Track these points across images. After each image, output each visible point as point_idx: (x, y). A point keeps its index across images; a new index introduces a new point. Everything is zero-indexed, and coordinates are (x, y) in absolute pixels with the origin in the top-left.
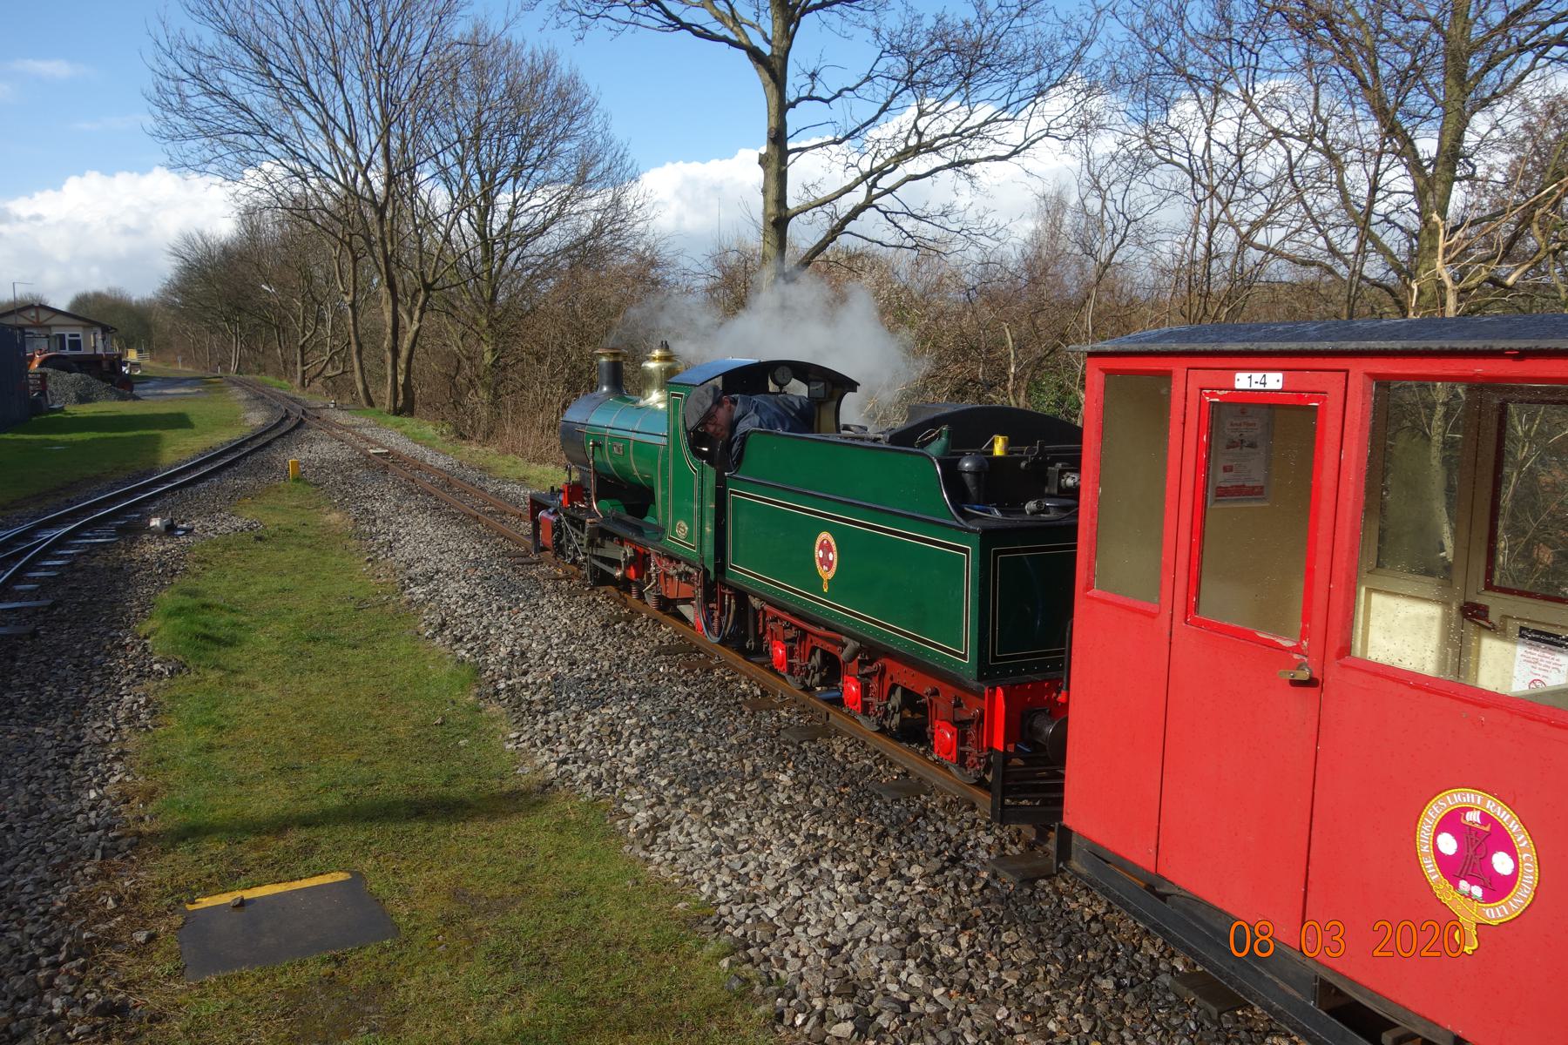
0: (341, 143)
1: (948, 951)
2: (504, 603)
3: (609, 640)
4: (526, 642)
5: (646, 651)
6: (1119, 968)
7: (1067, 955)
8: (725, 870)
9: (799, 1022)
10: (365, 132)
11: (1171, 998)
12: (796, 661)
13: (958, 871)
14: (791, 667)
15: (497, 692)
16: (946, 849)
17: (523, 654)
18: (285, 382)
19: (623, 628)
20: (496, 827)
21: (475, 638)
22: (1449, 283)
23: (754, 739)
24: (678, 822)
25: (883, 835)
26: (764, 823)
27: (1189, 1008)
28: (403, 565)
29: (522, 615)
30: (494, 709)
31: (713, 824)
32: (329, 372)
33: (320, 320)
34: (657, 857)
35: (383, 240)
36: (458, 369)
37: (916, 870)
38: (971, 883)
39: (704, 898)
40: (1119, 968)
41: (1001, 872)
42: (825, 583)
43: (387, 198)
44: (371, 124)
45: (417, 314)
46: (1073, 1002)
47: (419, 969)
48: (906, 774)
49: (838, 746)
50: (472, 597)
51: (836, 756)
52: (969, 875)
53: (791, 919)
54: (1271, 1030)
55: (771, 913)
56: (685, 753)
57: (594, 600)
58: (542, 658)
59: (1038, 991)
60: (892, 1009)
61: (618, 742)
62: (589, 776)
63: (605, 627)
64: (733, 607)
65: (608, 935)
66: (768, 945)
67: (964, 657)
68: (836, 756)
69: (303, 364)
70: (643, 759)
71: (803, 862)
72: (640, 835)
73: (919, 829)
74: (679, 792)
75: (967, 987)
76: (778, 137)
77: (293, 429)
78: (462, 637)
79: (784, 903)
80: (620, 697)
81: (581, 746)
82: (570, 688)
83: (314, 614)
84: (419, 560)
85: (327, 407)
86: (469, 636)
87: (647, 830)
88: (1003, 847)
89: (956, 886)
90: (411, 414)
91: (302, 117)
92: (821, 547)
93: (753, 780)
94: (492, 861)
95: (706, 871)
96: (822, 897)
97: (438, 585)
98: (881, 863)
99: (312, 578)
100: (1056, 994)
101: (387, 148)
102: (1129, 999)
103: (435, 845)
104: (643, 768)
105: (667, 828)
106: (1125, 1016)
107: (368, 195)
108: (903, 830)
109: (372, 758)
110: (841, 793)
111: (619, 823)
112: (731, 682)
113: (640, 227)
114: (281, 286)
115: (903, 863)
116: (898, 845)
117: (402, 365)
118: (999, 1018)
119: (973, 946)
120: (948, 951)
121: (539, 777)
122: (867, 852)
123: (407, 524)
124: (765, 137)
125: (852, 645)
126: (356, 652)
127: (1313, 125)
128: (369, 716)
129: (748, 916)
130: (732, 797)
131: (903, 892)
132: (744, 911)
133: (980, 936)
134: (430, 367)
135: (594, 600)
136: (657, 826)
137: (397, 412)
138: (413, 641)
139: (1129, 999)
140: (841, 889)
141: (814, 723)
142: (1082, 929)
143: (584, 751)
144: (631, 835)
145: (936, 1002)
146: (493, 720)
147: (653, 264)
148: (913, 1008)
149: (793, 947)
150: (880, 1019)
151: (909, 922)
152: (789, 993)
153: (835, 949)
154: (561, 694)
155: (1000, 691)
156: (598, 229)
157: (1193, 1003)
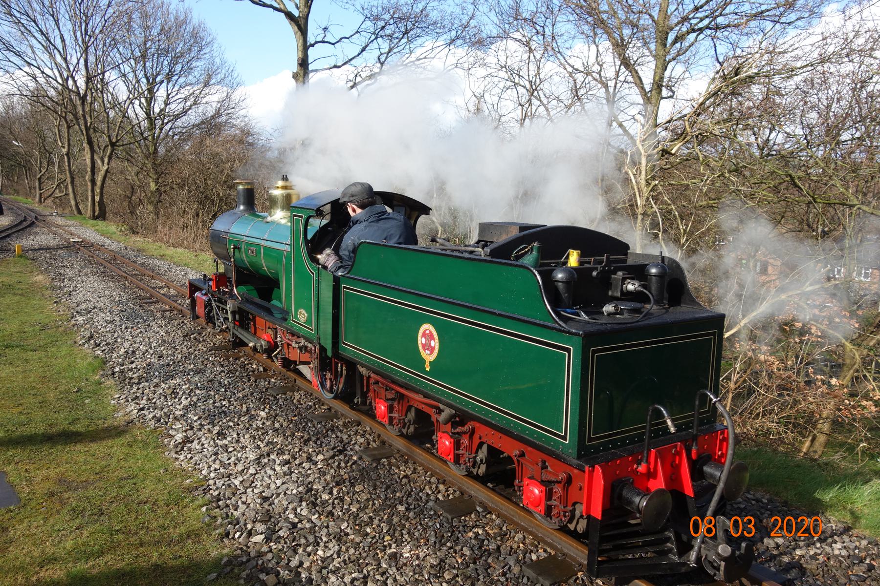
0: (59, 59)
1: (325, 496)
2: (130, 324)
3: (185, 343)
4: (136, 345)
5: (205, 349)
6: (410, 500)
7: (386, 495)
8: (218, 462)
9: (237, 536)
10: (74, 51)
11: (432, 513)
12: (395, 415)
13: (341, 457)
14: (391, 420)
15: (113, 373)
16: (338, 446)
17: (133, 352)
18: (30, 200)
19: (195, 337)
20: (94, 446)
21: (108, 344)
22: (643, 152)
23: (252, 394)
24: (198, 439)
25: (309, 440)
26: (246, 437)
27: (439, 517)
28: (75, 304)
29: (139, 331)
30: (110, 382)
31: (218, 439)
32: (58, 194)
33: (50, 162)
34: (182, 457)
35: (84, 116)
36: (133, 192)
37: (320, 457)
38: (347, 462)
39: (201, 477)
40: (410, 500)
41: (364, 456)
42: (427, 364)
43: (86, 91)
44: (77, 46)
45: (106, 160)
46: (383, 518)
47: (26, 520)
48: (330, 409)
49: (297, 395)
50: (111, 322)
51: (295, 401)
52: (347, 458)
53: (248, 485)
54: (476, 525)
55: (237, 482)
56: (211, 402)
57: (183, 322)
58: (144, 354)
59: (366, 514)
60: (287, 527)
61: (175, 398)
62: (154, 416)
63: (185, 336)
64: (344, 372)
65: (141, 498)
66: (231, 499)
67: (564, 438)
68: (295, 401)
69: (40, 189)
70: (187, 406)
71: (262, 456)
72: (176, 446)
73: (328, 436)
74: (203, 423)
75: (331, 514)
76: (304, 63)
77: (26, 228)
78: (100, 344)
79: (245, 477)
80: (183, 374)
81: (154, 401)
82: (156, 370)
83: (14, 332)
84: (85, 302)
85: (52, 215)
86: (104, 343)
87: (180, 443)
88: (369, 444)
89: (339, 464)
90: (104, 219)
91: (34, 42)
92: (424, 335)
93: (245, 415)
94: (85, 463)
95: (207, 463)
96: (266, 473)
97: (93, 315)
98: (303, 455)
99: (17, 313)
100: (375, 515)
101: (86, 61)
102: (411, 515)
103: (54, 456)
104: (186, 411)
105: (192, 442)
106: (406, 523)
107: (74, 88)
108: (319, 438)
109: (29, 411)
110: (292, 420)
111: (166, 440)
112: (248, 364)
113: (242, 113)
114: (26, 142)
115: (314, 454)
116: (314, 445)
117: (98, 190)
118: (342, 528)
119: (339, 493)
120: (325, 496)
121: (126, 418)
122: (297, 449)
123: (83, 282)
124: (296, 63)
125: (447, 412)
126: (35, 353)
127: (791, 72)
128: (33, 388)
129: (223, 485)
130: (231, 424)
131: (310, 469)
132: (222, 482)
133: (344, 488)
134: (115, 190)
135: (183, 322)
136: (187, 440)
137: (95, 218)
138: (71, 346)
139: (411, 515)
140: (278, 468)
141: (288, 385)
142: (397, 482)
143: (155, 403)
144: (171, 447)
145: (312, 522)
146: (108, 389)
147: (249, 134)
148: (299, 526)
149: (244, 499)
150: (280, 533)
151: (309, 483)
152: (235, 522)
153: (265, 499)
154: (150, 373)
155: (598, 469)
156: (218, 113)
157: (441, 514)
